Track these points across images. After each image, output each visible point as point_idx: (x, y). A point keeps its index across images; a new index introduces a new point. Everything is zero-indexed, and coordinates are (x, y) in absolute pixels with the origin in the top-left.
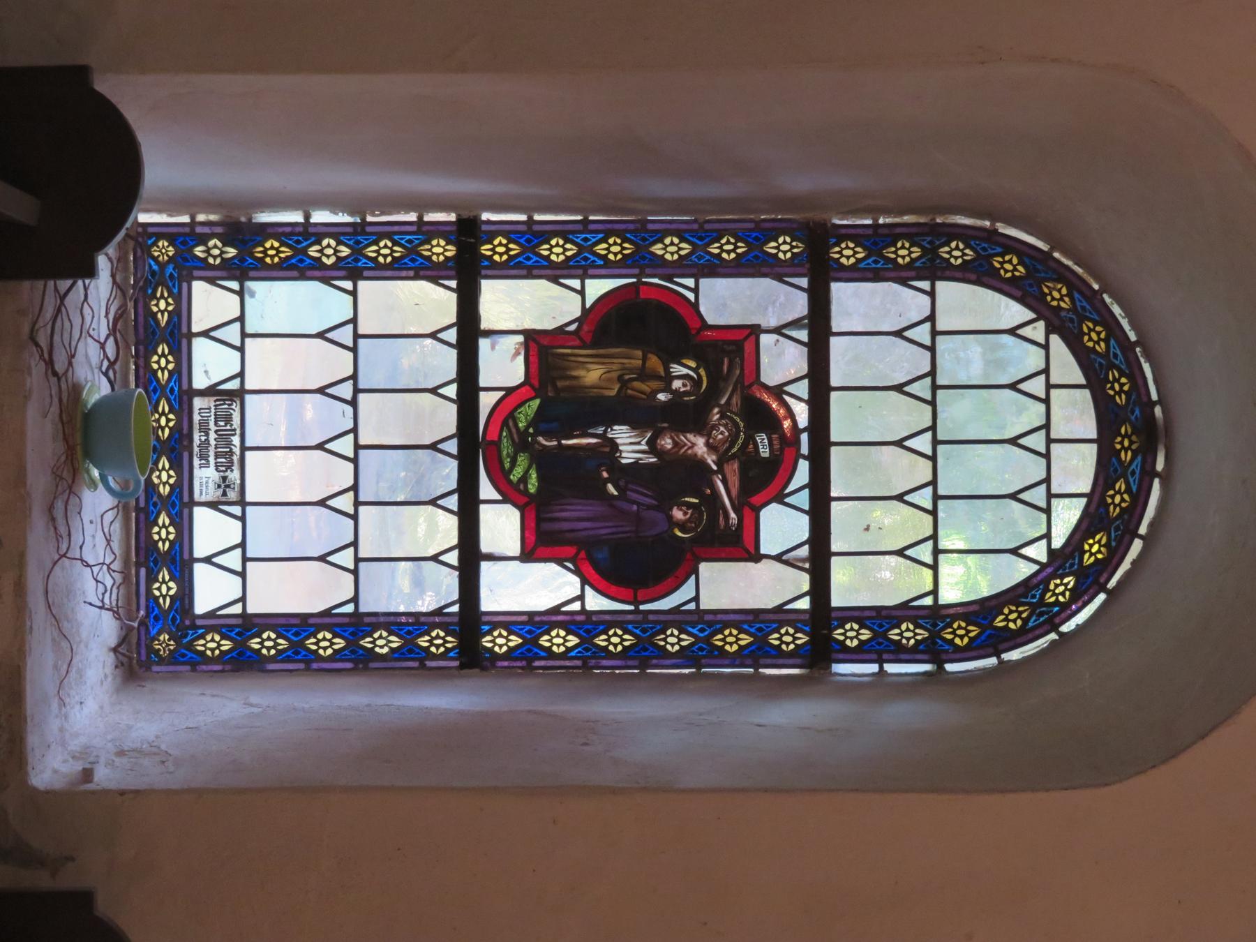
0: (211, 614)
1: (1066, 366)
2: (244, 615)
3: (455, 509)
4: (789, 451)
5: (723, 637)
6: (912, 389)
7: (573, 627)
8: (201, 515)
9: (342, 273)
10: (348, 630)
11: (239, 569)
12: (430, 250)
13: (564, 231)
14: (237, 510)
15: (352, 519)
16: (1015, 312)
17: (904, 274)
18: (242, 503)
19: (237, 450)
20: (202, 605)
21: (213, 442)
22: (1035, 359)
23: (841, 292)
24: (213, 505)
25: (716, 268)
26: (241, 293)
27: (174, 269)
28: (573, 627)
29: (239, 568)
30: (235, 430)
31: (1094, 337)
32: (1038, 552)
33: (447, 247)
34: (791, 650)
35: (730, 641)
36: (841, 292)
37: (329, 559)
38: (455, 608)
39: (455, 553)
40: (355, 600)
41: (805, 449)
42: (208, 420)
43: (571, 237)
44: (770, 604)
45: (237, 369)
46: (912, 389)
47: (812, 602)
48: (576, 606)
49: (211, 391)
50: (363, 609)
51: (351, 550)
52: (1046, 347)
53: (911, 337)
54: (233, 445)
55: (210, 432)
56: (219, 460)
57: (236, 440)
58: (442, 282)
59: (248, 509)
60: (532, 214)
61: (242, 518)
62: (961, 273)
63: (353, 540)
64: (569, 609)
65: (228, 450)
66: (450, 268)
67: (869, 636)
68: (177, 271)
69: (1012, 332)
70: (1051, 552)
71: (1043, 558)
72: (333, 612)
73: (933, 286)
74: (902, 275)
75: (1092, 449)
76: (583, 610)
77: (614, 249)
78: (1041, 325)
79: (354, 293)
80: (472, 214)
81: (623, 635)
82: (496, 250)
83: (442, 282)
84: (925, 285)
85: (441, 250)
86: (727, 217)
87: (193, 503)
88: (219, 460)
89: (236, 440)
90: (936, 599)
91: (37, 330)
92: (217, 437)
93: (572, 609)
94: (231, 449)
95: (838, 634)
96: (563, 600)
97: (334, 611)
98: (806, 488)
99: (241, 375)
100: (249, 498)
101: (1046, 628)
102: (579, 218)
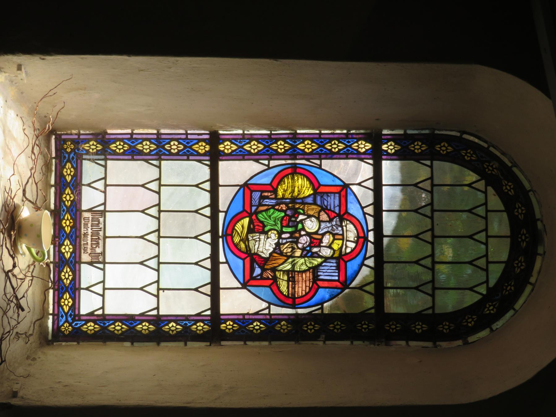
1: (495, 202)
2: (103, 315)
5: (226, 325)
6: (477, 211)
7: (263, 321)
8: (85, 268)
9: (369, 157)
10: (61, 319)
11: (102, 293)
12: (312, 146)
13: (339, 139)
14: (101, 266)
16: (471, 177)
17: (363, 156)
18: (104, 263)
19: (101, 238)
20: (84, 310)
21: (90, 234)
23: (223, 165)
24: (91, 264)
25: (331, 155)
26: (431, 167)
27: (74, 155)
28: (263, 321)
30: (101, 228)
31: (508, 187)
32: (483, 290)
33: (395, 146)
34: (259, 333)
35: (230, 326)
38: (209, 313)
40: (103, 308)
42: (88, 223)
43: (341, 140)
45: (103, 201)
46: (477, 211)
47: (211, 312)
48: (266, 311)
49: (90, 210)
50: (107, 312)
51: (156, 284)
52: (485, 192)
54: (100, 235)
55: (89, 229)
56: (93, 242)
57: (101, 233)
60: (296, 130)
61: (103, 270)
65: (97, 237)
66: (369, 154)
68: (75, 155)
70: (488, 289)
73: (432, 163)
75: (509, 240)
76: (269, 314)
78: (483, 182)
79: (159, 167)
80: (216, 130)
81: (260, 325)
82: (226, 147)
84: (428, 163)
85: (202, 148)
86: (235, 132)
87: (80, 262)
88: (93, 242)
89: (101, 233)
90: (433, 311)
92: (92, 231)
94: (99, 237)
99: (104, 204)
100: (107, 261)
101: (107, 318)
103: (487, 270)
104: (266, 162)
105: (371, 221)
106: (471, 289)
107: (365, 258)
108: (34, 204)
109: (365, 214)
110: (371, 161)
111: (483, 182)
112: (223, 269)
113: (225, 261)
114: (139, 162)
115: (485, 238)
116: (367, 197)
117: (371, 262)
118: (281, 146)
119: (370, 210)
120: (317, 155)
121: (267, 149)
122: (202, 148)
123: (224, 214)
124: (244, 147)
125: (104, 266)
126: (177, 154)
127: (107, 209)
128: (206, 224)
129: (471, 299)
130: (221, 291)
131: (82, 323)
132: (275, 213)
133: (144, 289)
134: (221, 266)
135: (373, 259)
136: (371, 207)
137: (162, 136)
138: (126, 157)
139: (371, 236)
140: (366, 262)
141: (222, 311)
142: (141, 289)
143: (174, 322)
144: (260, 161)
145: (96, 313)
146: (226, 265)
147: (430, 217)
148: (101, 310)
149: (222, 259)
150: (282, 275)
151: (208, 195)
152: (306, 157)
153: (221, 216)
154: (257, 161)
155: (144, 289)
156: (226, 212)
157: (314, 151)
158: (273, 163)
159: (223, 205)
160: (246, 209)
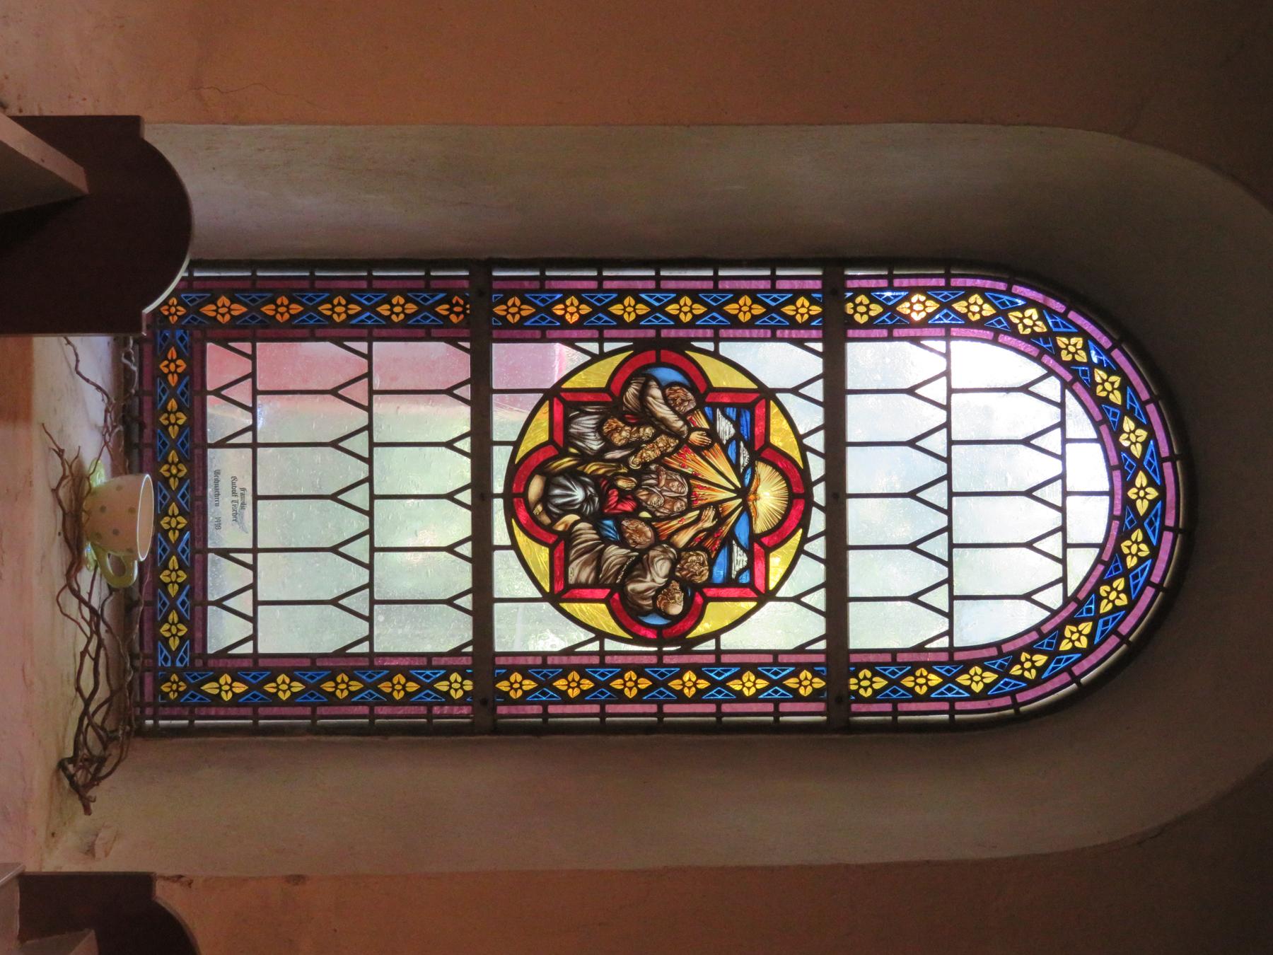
0: (223, 653)
1: (1079, 424)
14: (248, 558)
15: (250, 569)
22: (1053, 415)
23: (499, 352)
29: (1060, 555)
32: (1054, 598)
36: (499, 352)
38: (822, 645)
47: (828, 644)
50: (378, 648)
52: (1062, 405)
53: (809, 394)
59: (260, 556)
69: (1025, 389)
70: (1067, 600)
74: (339, 334)
85: (803, 309)
97: (349, 651)
102: (422, 274)
103: (1063, 561)
104: (593, 347)
105: (817, 467)
106: (1028, 597)
107: (805, 540)
108: (191, 428)
109: (804, 449)
110: (819, 347)
113: (508, 542)
116: (809, 417)
117: (818, 547)
119: (817, 441)
120: (652, 328)
121: (945, 311)
124: (897, 309)
125: (255, 559)
126: (750, 325)
127: (260, 440)
128: (459, 470)
129: (1024, 617)
132: (93, 461)
133: (455, 602)
134: (497, 555)
135: (822, 540)
136: (821, 435)
139: (819, 494)
140: (807, 547)
141: (854, 644)
146: (512, 553)
148: (250, 644)
150: (611, 570)
151: (466, 411)
154: (570, 342)
155: (455, 602)
157: (814, 321)
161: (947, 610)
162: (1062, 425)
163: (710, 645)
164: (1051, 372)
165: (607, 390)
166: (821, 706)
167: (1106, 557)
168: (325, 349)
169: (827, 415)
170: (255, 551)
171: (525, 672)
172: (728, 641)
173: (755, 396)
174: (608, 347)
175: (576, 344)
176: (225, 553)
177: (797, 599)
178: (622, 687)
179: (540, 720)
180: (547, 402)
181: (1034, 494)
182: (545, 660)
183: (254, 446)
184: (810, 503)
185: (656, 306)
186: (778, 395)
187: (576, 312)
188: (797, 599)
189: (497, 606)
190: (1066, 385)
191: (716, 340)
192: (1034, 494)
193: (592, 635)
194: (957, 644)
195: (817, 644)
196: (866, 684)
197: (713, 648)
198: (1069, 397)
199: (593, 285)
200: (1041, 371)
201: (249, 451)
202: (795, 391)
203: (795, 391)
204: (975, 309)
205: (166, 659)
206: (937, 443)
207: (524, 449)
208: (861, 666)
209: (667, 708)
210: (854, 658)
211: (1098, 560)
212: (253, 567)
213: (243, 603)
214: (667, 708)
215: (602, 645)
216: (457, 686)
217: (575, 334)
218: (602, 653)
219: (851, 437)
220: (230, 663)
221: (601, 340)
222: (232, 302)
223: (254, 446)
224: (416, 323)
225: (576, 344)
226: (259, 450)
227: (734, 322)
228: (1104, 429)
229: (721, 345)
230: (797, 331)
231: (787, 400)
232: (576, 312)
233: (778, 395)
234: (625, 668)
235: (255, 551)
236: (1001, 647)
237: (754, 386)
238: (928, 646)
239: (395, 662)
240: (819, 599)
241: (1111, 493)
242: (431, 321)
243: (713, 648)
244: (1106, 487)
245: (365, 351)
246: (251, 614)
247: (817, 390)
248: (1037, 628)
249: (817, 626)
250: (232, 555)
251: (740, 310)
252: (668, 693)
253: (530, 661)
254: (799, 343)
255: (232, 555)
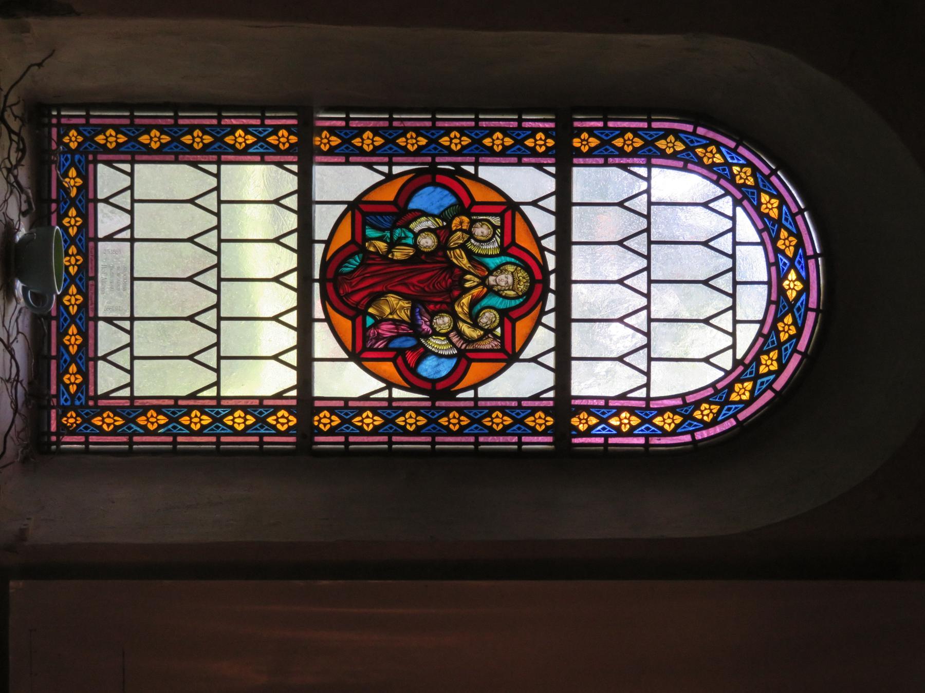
0: (106, 396)
1: (747, 230)
3: (295, 324)
4: (539, 288)
23: (578, 174)
32: (726, 361)
37: (196, 358)
38: (551, 394)
39: (294, 353)
41: (552, 286)
44: (185, 392)
47: (556, 394)
52: (733, 219)
58: (411, 175)
62: (406, 125)
63: (129, 342)
64: (202, 395)
67: (424, 422)
70: (736, 363)
71: (729, 367)
72: (371, 397)
77: (412, 142)
83: (411, 175)
85: (541, 142)
91: (12, 192)
93: (412, 393)
95: (293, 421)
96: (628, 389)
98: (553, 312)
103: (733, 334)
104: (385, 169)
106: (707, 360)
107: (543, 313)
110: (552, 170)
111: (728, 199)
112: (321, 332)
114: (269, 166)
115: (731, 287)
116: (544, 223)
117: (550, 319)
118: (412, 142)
119: (550, 243)
121: (476, 145)
122: (541, 142)
123: (323, 246)
126: (159, 151)
129: (708, 376)
130: (574, 363)
131: (209, 410)
135: (553, 315)
137: (525, 125)
138: (336, 159)
141: (317, 392)
142: (191, 357)
143: (242, 410)
144: (200, 166)
145: (545, 396)
146: (326, 324)
147: (215, 252)
149: (318, 312)
152: (624, 161)
153: (319, 250)
154: (369, 166)
156: (328, 243)
158: (396, 170)
159: (321, 231)
160: (356, 239)
161: (646, 371)
162: (733, 230)
163: (470, 394)
164: (727, 193)
165: (394, 203)
166: (549, 439)
167: (766, 331)
168: (615, 173)
169: (558, 223)
170: (132, 319)
171: (159, 410)
172: (484, 392)
173: (504, 207)
174: (396, 170)
175: (544, 168)
176: (109, 320)
177: (534, 360)
178: (146, 422)
179: (429, 446)
180: (350, 212)
181: (710, 283)
182: (261, 402)
183: (132, 240)
184: (547, 290)
185: (648, 140)
186: (522, 207)
187: (287, 142)
188: (534, 360)
189: (316, 364)
190: (737, 203)
191: (476, 165)
192: (710, 283)
193: (383, 385)
194: (653, 394)
195: (379, 394)
196: (325, 420)
197: (472, 396)
198: (739, 210)
199: (386, 124)
200: (720, 192)
201: (136, 244)
202: (534, 203)
203: (534, 203)
204: (112, 139)
205: (66, 400)
206: (725, 244)
207: (334, 248)
208: (321, 409)
209: (352, 439)
210: (317, 404)
211: (759, 334)
212: (130, 332)
213: (123, 359)
214: (352, 439)
215: (390, 393)
216: (541, 421)
217: (199, 158)
218: (390, 399)
219: (575, 238)
220: (200, 402)
221: (390, 164)
222: (161, 134)
223: (132, 240)
224: (643, 154)
225: (544, 168)
226: (129, 244)
227: (491, 152)
228: (765, 235)
229: (481, 168)
230: (626, 159)
231: (528, 210)
232: (287, 142)
233: (522, 207)
234: (407, 409)
235: (132, 319)
236: (685, 398)
237: (502, 200)
238: (629, 395)
239: (493, 404)
240: (550, 360)
241: (769, 283)
242: (95, 149)
243: (472, 396)
244: (765, 279)
245: (129, 170)
246: (129, 368)
247: (551, 203)
248: (713, 385)
249: (548, 379)
250: (115, 322)
251: (159, 138)
252: (653, 428)
253: (250, 402)
254: (539, 167)
255: (115, 322)
